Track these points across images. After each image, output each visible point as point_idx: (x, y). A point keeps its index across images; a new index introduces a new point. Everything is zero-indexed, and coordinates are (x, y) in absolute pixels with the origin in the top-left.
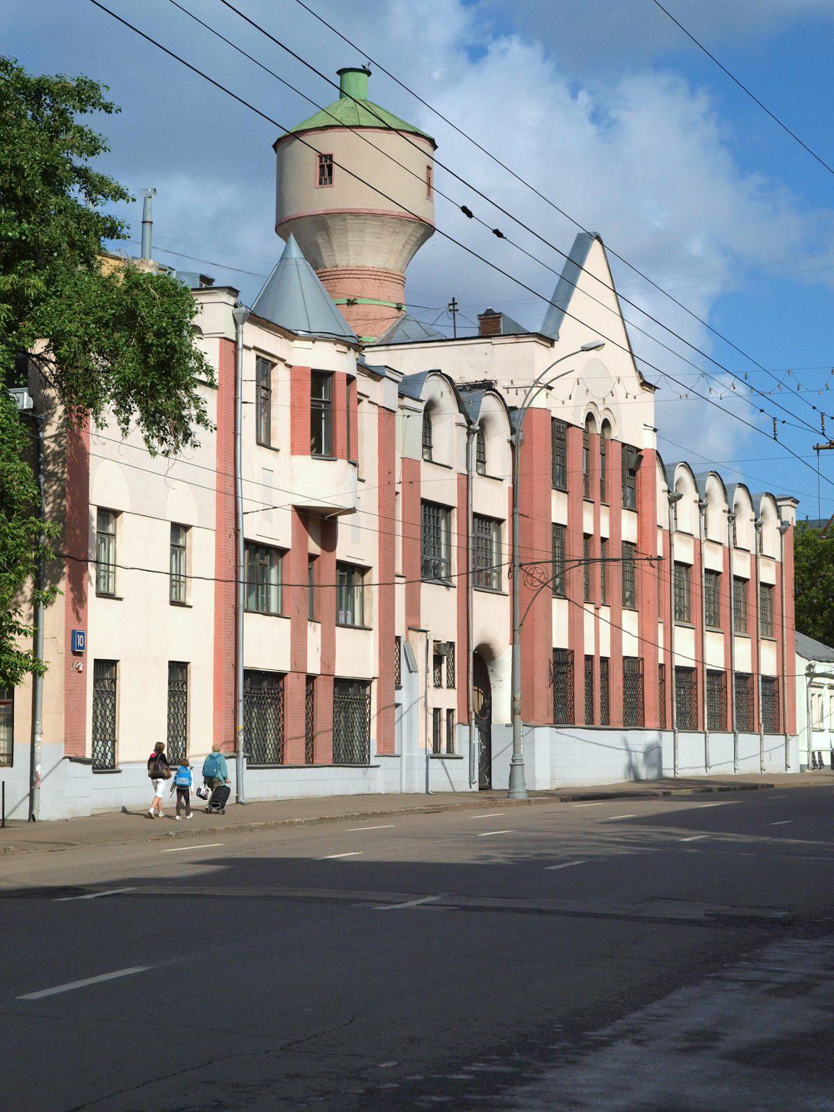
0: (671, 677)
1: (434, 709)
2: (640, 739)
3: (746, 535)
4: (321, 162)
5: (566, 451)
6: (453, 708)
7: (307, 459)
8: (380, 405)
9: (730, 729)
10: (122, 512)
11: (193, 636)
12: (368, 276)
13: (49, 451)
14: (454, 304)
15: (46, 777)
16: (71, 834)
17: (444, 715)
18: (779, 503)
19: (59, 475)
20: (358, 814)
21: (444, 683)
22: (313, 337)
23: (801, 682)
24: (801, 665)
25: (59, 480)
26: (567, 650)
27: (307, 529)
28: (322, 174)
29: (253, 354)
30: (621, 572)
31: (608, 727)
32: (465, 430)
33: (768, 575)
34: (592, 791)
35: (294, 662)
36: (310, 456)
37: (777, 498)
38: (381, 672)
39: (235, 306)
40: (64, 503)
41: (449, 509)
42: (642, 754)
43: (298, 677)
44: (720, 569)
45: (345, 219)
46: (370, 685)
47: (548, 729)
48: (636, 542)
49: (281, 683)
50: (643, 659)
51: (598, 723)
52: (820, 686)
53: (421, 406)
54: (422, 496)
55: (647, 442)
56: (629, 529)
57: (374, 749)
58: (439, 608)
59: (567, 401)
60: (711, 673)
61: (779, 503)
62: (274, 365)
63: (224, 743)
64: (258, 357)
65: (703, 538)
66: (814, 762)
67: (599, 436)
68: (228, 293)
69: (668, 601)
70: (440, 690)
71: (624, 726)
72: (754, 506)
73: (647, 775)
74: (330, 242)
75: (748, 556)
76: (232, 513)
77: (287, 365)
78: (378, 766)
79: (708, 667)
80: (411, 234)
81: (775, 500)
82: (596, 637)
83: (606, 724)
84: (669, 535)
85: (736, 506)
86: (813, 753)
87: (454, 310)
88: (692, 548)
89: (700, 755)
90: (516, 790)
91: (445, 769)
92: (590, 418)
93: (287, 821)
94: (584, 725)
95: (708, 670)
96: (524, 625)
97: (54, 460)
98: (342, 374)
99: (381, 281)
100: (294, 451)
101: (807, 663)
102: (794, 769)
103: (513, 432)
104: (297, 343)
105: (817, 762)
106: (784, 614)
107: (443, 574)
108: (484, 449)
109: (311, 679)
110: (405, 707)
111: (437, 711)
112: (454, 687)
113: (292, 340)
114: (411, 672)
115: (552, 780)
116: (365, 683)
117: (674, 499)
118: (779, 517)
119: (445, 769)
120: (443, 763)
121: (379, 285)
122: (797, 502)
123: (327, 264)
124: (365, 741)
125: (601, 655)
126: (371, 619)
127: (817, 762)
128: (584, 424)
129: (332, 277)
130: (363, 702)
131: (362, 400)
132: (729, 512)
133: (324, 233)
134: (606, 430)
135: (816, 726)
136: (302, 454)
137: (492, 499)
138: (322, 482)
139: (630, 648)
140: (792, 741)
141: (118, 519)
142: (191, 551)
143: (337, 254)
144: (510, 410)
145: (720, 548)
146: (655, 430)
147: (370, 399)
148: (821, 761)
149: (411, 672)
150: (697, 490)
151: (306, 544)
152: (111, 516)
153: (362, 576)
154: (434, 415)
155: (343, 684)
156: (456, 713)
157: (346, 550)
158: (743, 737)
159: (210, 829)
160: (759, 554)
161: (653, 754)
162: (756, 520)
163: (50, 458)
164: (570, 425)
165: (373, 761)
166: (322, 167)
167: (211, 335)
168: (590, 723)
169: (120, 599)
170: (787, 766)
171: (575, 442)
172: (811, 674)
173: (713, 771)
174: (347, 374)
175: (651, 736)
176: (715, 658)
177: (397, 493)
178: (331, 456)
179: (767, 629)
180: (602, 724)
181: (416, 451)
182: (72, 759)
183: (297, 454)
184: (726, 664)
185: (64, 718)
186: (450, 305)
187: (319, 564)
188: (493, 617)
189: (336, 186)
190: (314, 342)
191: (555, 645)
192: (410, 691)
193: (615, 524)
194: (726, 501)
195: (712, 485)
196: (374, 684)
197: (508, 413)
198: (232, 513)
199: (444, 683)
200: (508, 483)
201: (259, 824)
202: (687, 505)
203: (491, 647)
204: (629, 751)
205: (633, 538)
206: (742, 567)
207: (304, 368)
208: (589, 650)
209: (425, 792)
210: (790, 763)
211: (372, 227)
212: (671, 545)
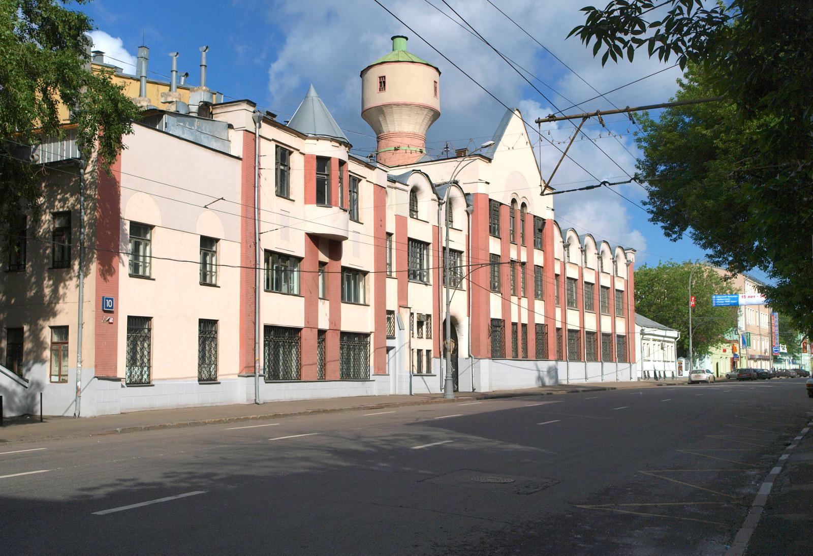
0: (565, 335)
1: (418, 350)
2: (544, 365)
3: (608, 265)
4: (380, 80)
5: (493, 215)
8: (375, 183)
9: (599, 360)
10: (155, 226)
11: (224, 303)
13: (87, 182)
14: (447, 148)
15: (84, 389)
16: (104, 426)
17: (424, 353)
18: (626, 252)
19: (93, 196)
20: (310, 411)
21: (424, 336)
23: (638, 337)
24: (638, 329)
25: (93, 199)
26: (500, 320)
27: (318, 247)
28: (381, 86)
29: (273, 144)
30: (537, 282)
31: (526, 359)
32: (437, 203)
33: (620, 285)
34: (510, 392)
35: (307, 320)
36: (316, 205)
37: (624, 249)
38: (376, 329)
39: (254, 112)
40: (96, 214)
41: (428, 244)
42: (546, 373)
43: (311, 331)
44: (594, 282)
45: (392, 108)
46: (217, 323)
47: (487, 360)
48: (543, 266)
49: (300, 333)
50: (547, 325)
51: (520, 358)
52: (649, 340)
53: (409, 189)
55: (548, 215)
56: (538, 258)
57: (372, 372)
58: (421, 298)
60: (619, 336)
61: (626, 252)
62: (360, 180)
63: (246, 367)
64: (277, 146)
65: (567, 260)
66: (645, 376)
68: (247, 104)
69: (564, 297)
70: (422, 339)
71: (536, 358)
72: (612, 251)
74: (385, 119)
75: (609, 276)
76: (251, 235)
77: (301, 153)
78: (374, 381)
79: (586, 330)
80: (426, 115)
81: (623, 250)
82: (519, 311)
83: (526, 358)
84: (564, 265)
85: (602, 252)
86: (644, 372)
89: (577, 373)
90: (448, 394)
91: (424, 381)
92: (514, 201)
93: (242, 417)
94: (511, 358)
95: (586, 331)
96: (476, 307)
97: (90, 187)
98: (335, 159)
101: (641, 328)
102: (634, 379)
103: (468, 206)
104: (307, 141)
105: (647, 376)
106: (629, 303)
107: (425, 279)
108: (452, 214)
109: (322, 333)
110: (397, 348)
111: (419, 351)
112: (431, 338)
113: (305, 139)
114: (400, 330)
115: (490, 386)
116: (367, 335)
117: (566, 246)
118: (626, 258)
119: (424, 381)
120: (423, 378)
122: (635, 251)
123: (385, 131)
124: (367, 366)
125: (522, 322)
126: (369, 299)
127: (647, 376)
128: (510, 203)
130: (366, 345)
131: (361, 180)
132: (598, 254)
133: (382, 115)
134: (524, 208)
135: (646, 358)
136: (311, 204)
137: (458, 242)
138: (328, 221)
139: (540, 319)
140: (633, 366)
141: (153, 231)
142: (219, 254)
143: (389, 126)
144: (466, 195)
145: (594, 272)
146: (553, 210)
147: (367, 179)
148: (649, 376)
149: (400, 330)
150: (580, 243)
151: (317, 255)
152: (215, 242)
153: (365, 276)
155: (347, 336)
156: (432, 352)
157: (348, 258)
158: (606, 364)
159: (160, 425)
160: (615, 276)
161: (553, 372)
162: (613, 259)
163: (88, 186)
164: (501, 204)
166: (380, 82)
167: (238, 129)
168: (515, 357)
169: (154, 280)
170: (631, 378)
171: (505, 214)
172: (642, 333)
173: (589, 381)
175: (552, 363)
176: (606, 328)
177: (390, 235)
178: (330, 205)
179: (620, 311)
180: (523, 358)
181: (406, 212)
182: (99, 378)
183: (308, 204)
184: (597, 328)
185: (94, 352)
187: (328, 268)
188: (458, 303)
190: (318, 140)
191: (492, 316)
192: (400, 340)
193: (530, 256)
194: (596, 249)
195: (588, 240)
196: (372, 336)
197: (465, 196)
198: (251, 235)
199: (424, 336)
200: (465, 232)
201: (213, 420)
202: (575, 248)
203: (456, 317)
204: (539, 371)
205: (541, 263)
206: (605, 281)
208: (515, 319)
209: (409, 394)
210: (633, 376)
211: (405, 110)
212: (565, 269)
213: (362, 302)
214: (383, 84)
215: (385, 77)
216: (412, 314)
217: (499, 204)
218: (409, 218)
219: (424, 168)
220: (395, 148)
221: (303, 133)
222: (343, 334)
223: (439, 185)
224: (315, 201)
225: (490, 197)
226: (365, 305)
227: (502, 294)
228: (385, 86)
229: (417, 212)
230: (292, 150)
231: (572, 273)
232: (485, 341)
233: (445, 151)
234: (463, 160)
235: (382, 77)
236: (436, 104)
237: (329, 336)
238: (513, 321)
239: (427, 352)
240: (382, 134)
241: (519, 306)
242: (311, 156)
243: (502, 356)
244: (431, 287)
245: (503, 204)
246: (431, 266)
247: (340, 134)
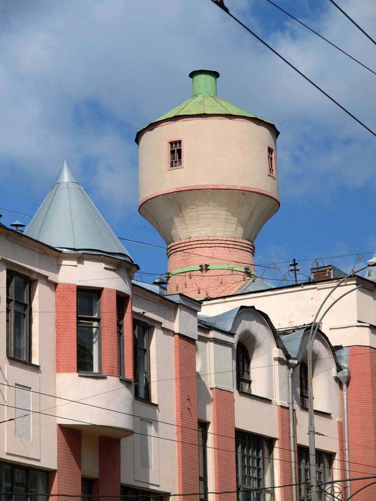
4: (172, 147)
7: (74, 376)
12: (218, 245)
14: (295, 264)
22: (82, 256)
28: (173, 158)
41: (271, 442)
54: (316, 447)
87: (295, 270)
98: (110, 290)
99: (230, 249)
100: (60, 368)
103: (339, 368)
121: (228, 252)
123: (182, 236)
129: (186, 248)
154: (249, 352)
166: (172, 152)
174: (117, 291)
186: (291, 265)
189: (185, 167)
200: (336, 418)
207: (69, 285)
214: (176, 155)
215: (180, 142)
218: (236, 394)
219: (261, 303)
220: (201, 266)
221: (54, 246)
223: (285, 333)
224: (76, 366)
228: (180, 157)
229: (249, 382)
233: (292, 270)
234: (338, 286)
236: (265, 185)
240: (174, 244)
246: (277, 483)
247: (113, 246)
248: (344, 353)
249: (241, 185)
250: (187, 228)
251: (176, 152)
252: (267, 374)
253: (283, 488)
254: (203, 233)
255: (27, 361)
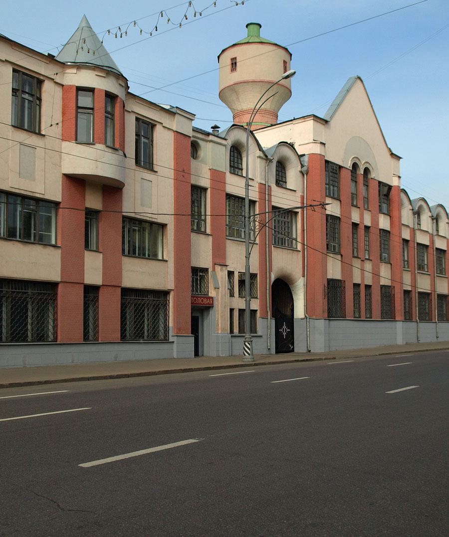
6: (255, 309)
8: (174, 130)
9: (414, 320)
22: (79, 66)
28: (232, 67)
38: (176, 287)
56: (384, 223)
57: (171, 333)
59: (154, 33)
67: (362, 176)
69: (414, 262)
73: (177, 356)
83: (369, 319)
88: (429, 238)
92: (355, 166)
98: (100, 90)
103: (302, 166)
116: (166, 293)
130: (165, 305)
139: (385, 281)
156: (258, 312)
164: (340, 167)
165: (171, 339)
168: (357, 319)
171: (345, 176)
174: (106, 91)
191: (330, 276)
200: (299, 194)
208: (357, 280)
213: (160, 257)
215: (236, 58)
216: (231, 274)
217: (338, 167)
222: (126, 292)
225: (326, 159)
226: (163, 260)
227: (342, 256)
230: (42, 78)
231: (423, 239)
232: (321, 302)
235: (234, 59)
237: (102, 295)
238: (355, 282)
239: (251, 314)
241: (362, 270)
242: (71, 87)
243: (343, 316)
244: (210, 238)
245: (343, 167)
248: (306, 159)
249: (267, 79)
250: (240, 104)
251: (234, 64)
252: (426, 222)
253: (176, 216)
254: (249, 106)
255: (112, 145)
